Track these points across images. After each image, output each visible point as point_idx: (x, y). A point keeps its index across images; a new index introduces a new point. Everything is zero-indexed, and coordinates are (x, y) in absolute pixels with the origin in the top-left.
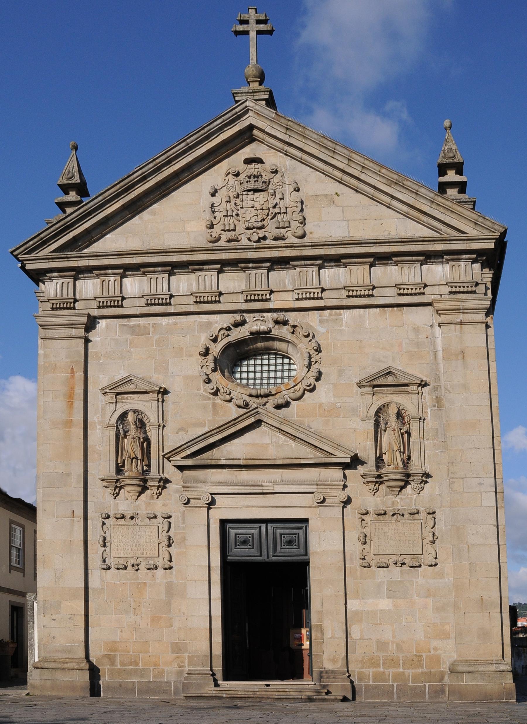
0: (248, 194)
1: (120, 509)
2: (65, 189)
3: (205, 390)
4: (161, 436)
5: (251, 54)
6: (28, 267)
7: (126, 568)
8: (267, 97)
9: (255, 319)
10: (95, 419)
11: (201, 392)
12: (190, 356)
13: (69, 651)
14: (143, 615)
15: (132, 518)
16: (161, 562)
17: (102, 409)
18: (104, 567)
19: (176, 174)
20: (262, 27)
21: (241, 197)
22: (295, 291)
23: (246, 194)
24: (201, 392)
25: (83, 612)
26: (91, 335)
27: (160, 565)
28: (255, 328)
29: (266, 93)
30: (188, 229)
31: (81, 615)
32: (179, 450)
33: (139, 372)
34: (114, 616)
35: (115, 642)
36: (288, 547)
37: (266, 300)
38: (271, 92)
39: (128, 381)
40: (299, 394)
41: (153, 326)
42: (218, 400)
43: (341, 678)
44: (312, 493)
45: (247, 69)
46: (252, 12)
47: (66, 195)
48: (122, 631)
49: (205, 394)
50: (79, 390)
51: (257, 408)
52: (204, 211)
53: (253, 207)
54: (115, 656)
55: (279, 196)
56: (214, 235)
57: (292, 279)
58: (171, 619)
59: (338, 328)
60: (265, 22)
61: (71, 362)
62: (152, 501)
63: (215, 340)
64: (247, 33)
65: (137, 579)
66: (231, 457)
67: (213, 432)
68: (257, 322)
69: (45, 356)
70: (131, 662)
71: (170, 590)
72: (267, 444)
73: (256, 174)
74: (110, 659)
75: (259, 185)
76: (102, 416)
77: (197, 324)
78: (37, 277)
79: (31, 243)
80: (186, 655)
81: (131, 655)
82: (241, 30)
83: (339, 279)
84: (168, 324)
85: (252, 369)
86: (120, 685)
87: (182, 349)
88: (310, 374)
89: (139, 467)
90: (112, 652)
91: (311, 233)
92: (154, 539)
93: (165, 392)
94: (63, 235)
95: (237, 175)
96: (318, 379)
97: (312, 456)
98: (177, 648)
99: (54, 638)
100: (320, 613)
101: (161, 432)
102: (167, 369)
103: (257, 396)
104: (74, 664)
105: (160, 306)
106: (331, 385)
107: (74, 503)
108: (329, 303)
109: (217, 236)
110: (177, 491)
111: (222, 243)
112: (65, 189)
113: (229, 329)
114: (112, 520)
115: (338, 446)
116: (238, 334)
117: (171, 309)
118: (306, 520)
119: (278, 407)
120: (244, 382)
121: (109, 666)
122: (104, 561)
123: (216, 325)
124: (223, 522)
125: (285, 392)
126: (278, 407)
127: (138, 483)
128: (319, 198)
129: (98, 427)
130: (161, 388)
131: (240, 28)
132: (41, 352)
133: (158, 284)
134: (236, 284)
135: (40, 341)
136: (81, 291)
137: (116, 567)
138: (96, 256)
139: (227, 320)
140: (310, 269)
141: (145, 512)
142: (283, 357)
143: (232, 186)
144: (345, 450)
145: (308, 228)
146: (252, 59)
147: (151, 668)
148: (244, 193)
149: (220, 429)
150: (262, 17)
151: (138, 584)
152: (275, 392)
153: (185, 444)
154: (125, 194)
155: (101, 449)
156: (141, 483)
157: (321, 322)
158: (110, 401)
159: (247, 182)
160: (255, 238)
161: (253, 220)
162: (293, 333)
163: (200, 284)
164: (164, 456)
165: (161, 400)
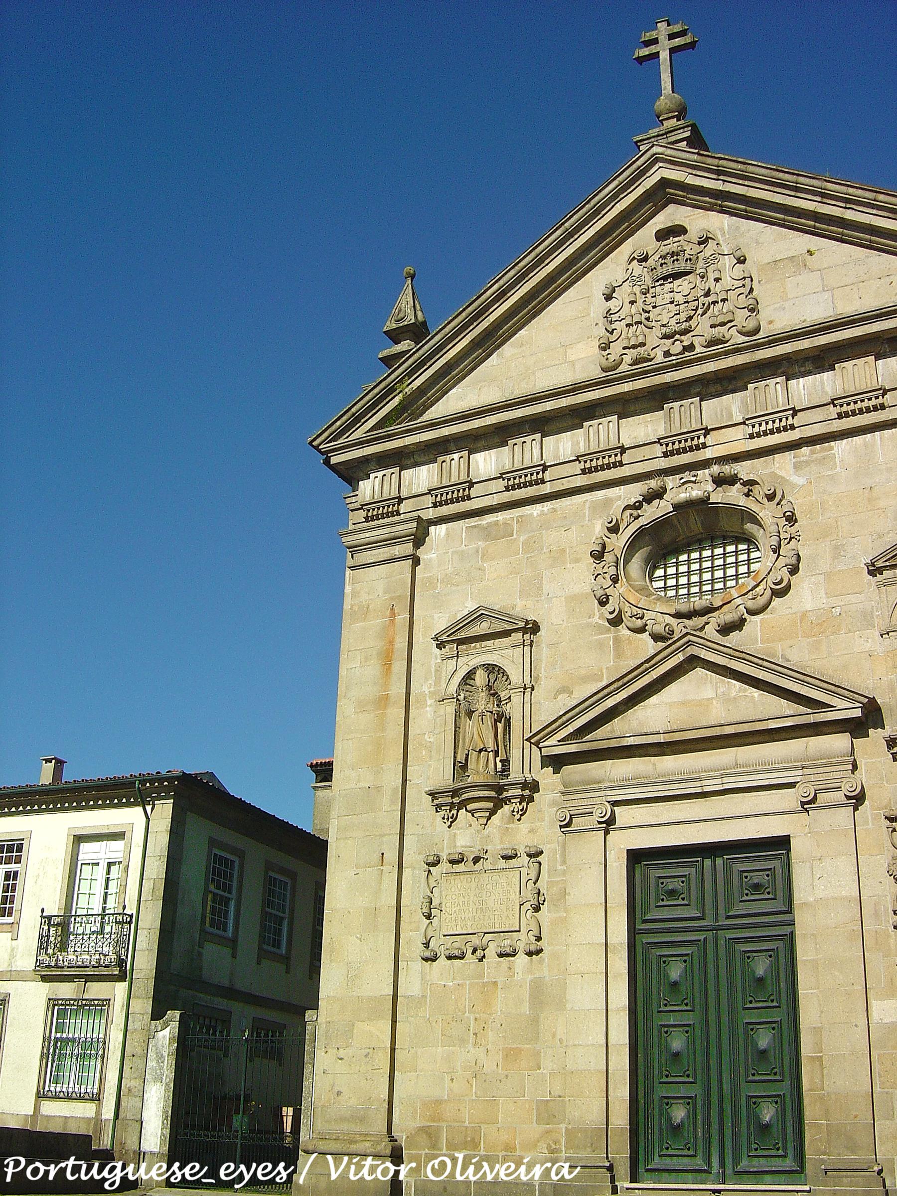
0: (663, 284)
1: (458, 844)
2: (395, 336)
3: (599, 616)
4: (527, 706)
5: (663, 82)
6: (334, 460)
7: (462, 957)
8: (688, 134)
9: (682, 481)
10: (426, 689)
11: (596, 619)
12: (577, 561)
13: (362, 1120)
14: (489, 1047)
15: (476, 860)
16: (523, 941)
17: (437, 671)
18: (427, 954)
19: (551, 279)
20: (678, 41)
21: (652, 290)
22: (747, 422)
23: (660, 285)
24: (596, 619)
25: (388, 1044)
26: (421, 553)
27: (521, 946)
28: (683, 496)
29: (686, 129)
30: (573, 358)
31: (385, 1048)
32: (554, 726)
33: (496, 601)
34: (440, 1049)
35: (438, 1102)
36: (753, 898)
37: (698, 448)
38: (694, 128)
39: (477, 616)
40: (761, 601)
41: (518, 522)
42: (623, 631)
43: (865, 1176)
44: (792, 785)
45: (658, 103)
46: (662, 26)
47: (396, 344)
48: (452, 1080)
49: (601, 622)
50: (401, 643)
51: (687, 634)
52: (597, 324)
53: (672, 302)
54: (439, 1129)
55: (712, 276)
56: (611, 358)
57: (742, 403)
58: (539, 1053)
59: (830, 473)
60: (682, 34)
61: (392, 599)
62: (510, 826)
63: (614, 529)
64: (656, 55)
65: (481, 976)
66: (643, 732)
67: (612, 688)
68: (686, 486)
69: (354, 595)
70: (466, 1142)
71: (539, 995)
72: (708, 699)
73: (675, 250)
74: (429, 1135)
75: (681, 266)
76: (435, 682)
77: (587, 505)
78: (352, 474)
79: (338, 423)
80: (563, 1126)
81: (467, 1127)
82: (647, 53)
83: (823, 388)
84: (542, 513)
85: (683, 569)
86: (445, 1189)
87: (564, 551)
88: (782, 561)
89: (491, 765)
90: (434, 1121)
91: (771, 322)
92: (513, 896)
93: (533, 628)
94: (384, 402)
95: (645, 259)
96: (794, 570)
97: (792, 713)
98: (548, 1112)
99: (339, 1093)
100: (817, 1031)
101: (527, 699)
102: (540, 588)
103: (689, 615)
104: (368, 1144)
105: (527, 489)
106: (822, 576)
107: (385, 839)
108: (808, 432)
109: (617, 358)
110: (554, 803)
111: (624, 367)
112: (395, 336)
113: (637, 506)
114: (444, 866)
115: (836, 689)
116: (653, 512)
117: (547, 489)
118: (783, 842)
119: (726, 629)
120: (671, 593)
121: (427, 1151)
122: (427, 945)
123: (619, 503)
124: (635, 857)
125: (739, 601)
126: (726, 629)
127: (487, 793)
128: (781, 265)
129: (429, 702)
130: (527, 622)
131: (645, 51)
132: (348, 589)
133: (525, 452)
134: (650, 428)
135: (348, 572)
136: (410, 484)
137: (447, 953)
138: (433, 425)
139: (633, 492)
140: (771, 382)
141: (499, 847)
142: (737, 540)
143: (640, 276)
144: (848, 693)
145: (764, 315)
146: (665, 88)
147: (500, 1154)
148: (658, 284)
149: (623, 680)
150: (677, 28)
151: (484, 985)
152: (721, 603)
153: (564, 714)
154: (475, 324)
155: (432, 740)
156: (493, 794)
157: (797, 467)
158: (450, 654)
159: (662, 265)
160: (677, 348)
161: (673, 322)
162: (747, 495)
163: (592, 440)
164: (528, 740)
165: (528, 642)
